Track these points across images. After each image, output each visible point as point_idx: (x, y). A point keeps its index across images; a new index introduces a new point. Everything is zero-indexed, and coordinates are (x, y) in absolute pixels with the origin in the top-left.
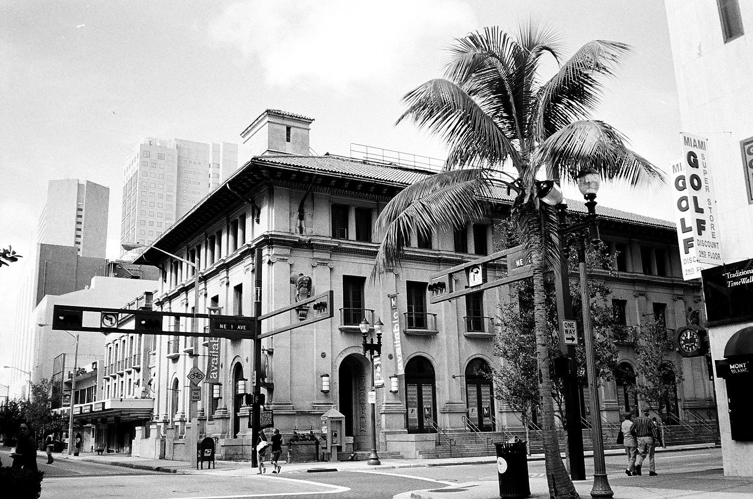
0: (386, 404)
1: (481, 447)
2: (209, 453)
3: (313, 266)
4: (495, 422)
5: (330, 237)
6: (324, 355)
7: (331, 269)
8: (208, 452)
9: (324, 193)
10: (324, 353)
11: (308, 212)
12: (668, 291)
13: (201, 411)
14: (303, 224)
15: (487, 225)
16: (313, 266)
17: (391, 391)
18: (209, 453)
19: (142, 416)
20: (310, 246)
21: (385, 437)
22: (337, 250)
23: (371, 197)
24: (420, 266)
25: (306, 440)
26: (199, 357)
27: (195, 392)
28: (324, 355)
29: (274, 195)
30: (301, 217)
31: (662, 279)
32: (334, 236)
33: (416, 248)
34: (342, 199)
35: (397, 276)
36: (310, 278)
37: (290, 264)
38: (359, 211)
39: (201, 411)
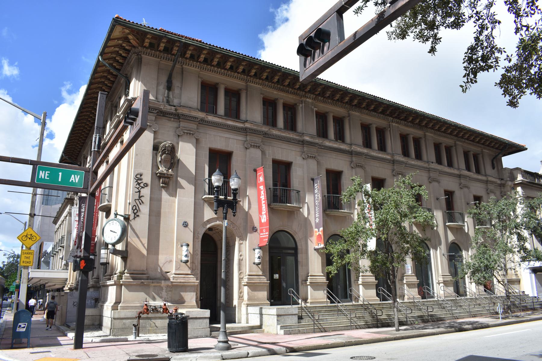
0: (175, 274)
1: (343, 321)
2: (24, 327)
3: (246, 148)
4: (466, 289)
5: (197, 109)
6: (186, 225)
7: (197, 140)
8: (23, 326)
9: (192, 68)
10: (186, 222)
11: (176, 83)
12: (241, 138)
13: (97, 278)
14: (171, 96)
15: (344, 117)
16: (179, 136)
17: (254, 263)
18: (24, 327)
19: (461, 290)
20: (177, 117)
21: (247, 309)
22: (202, 122)
23: (291, 92)
24: (285, 146)
25: (158, 312)
26: (35, 217)
27: (33, 253)
28: (186, 225)
29: (142, 64)
30: (169, 88)
31: (381, 155)
32: (202, 110)
33: (281, 129)
34: (273, 93)
35: (263, 153)
36: (173, 145)
37: (196, 139)
38: (228, 92)
39: (97, 278)
